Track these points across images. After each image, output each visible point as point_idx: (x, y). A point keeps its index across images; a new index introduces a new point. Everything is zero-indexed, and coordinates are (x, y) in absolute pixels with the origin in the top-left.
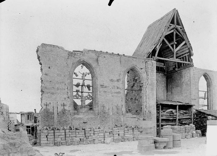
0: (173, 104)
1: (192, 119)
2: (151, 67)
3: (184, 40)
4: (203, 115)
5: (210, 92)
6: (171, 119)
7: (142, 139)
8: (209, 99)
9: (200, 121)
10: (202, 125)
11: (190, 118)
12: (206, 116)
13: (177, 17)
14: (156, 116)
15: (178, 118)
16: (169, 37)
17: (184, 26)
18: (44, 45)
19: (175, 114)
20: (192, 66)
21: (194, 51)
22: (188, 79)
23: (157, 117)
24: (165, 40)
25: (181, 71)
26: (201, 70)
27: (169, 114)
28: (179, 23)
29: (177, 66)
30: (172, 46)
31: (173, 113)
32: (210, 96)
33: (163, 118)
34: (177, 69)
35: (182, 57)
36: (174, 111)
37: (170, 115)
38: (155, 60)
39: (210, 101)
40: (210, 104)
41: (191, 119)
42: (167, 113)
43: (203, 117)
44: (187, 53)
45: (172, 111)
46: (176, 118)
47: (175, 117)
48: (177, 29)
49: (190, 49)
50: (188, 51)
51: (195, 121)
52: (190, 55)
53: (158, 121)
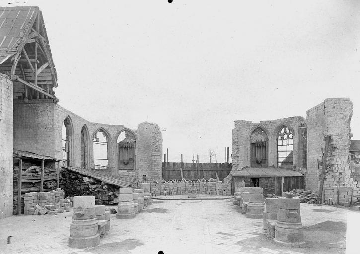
0: (38, 158)
1: (58, 181)
2: (6, 89)
3: (45, 61)
4: (74, 175)
5: (71, 142)
6: (35, 181)
7: (84, 227)
8: (70, 151)
9: (70, 184)
10: (72, 189)
11: (53, 180)
12: (80, 176)
13: (40, 23)
14: (12, 177)
15: (43, 180)
16: (29, 47)
17: (49, 40)
18: (38, 8)
19: (40, 173)
20: (53, 101)
21: (59, 82)
22: (49, 120)
23: (14, 179)
24: (24, 50)
25: (35, 105)
26: (65, 110)
27: (31, 174)
28: (43, 31)
29: (27, 96)
30: (33, 63)
31: (37, 172)
32: (71, 146)
33: (23, 180)
34: (26, 100)
35: (44, 83)
36: (38, 168)
37: (33, 176)
38: (14, 80)
39: (72, 153)
40: (72, 158)
41: (56, 181)
42: (28, 171)
43: (75, 179)
44: (49, 81)
45: (35, 169)
46: (40, 179)
47: (39, 178)
48: (39, 40)
49: (54, 77)
50: (50, 78)
51: (62, 184)
52: (54, 85)
53: (16, 183)
